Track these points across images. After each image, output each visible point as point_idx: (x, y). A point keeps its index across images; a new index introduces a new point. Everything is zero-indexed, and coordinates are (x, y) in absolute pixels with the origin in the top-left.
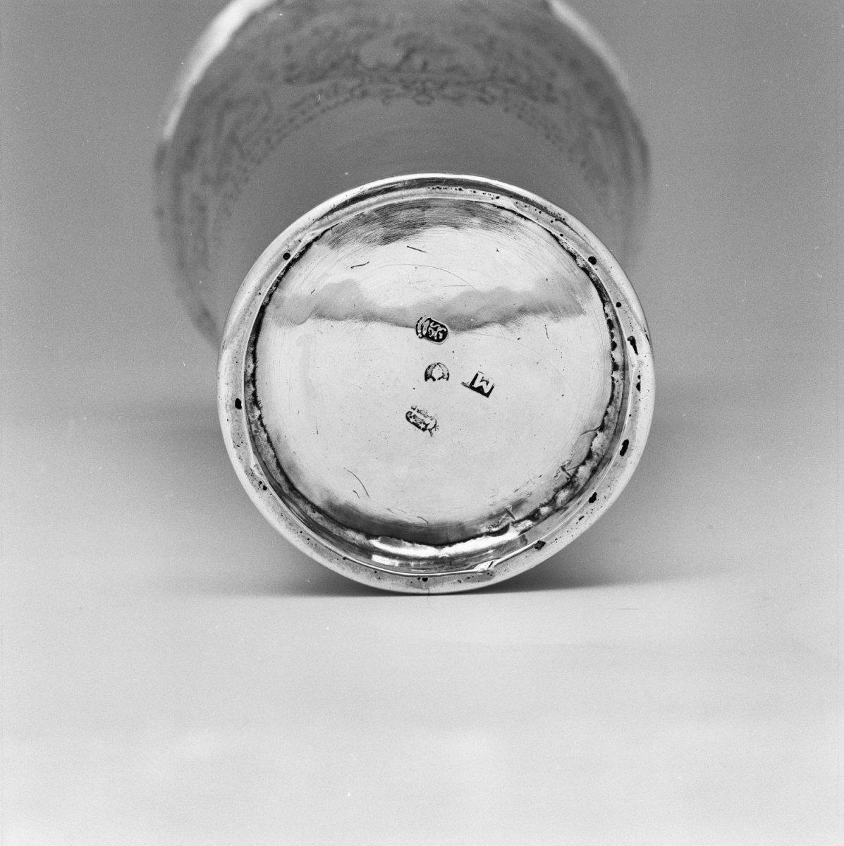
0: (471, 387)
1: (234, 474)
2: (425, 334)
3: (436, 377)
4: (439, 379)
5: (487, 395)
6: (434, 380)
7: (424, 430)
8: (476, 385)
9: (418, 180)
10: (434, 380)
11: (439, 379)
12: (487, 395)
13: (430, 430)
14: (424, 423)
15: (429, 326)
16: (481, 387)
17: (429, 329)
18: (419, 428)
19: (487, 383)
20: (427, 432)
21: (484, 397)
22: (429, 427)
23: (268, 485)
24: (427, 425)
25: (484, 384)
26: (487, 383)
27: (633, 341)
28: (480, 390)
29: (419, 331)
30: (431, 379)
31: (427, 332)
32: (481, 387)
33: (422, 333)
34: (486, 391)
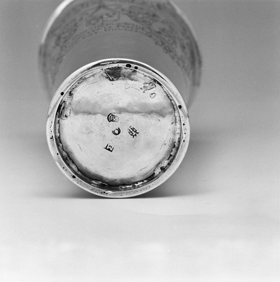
0: (106, 148)
1: (71, 74)
2: (120, 110)
3: (116, 130)
4: (115, 130)
5: (111, 151)
6: (116, 129)
7: (131, 135)
8: (108, 148)
9: (136, 63)
10: (116, 129)
11: (115, 130)
12: (111, 151)
13: (133, 136)
14: (132, 133)
15: (112, 117)
16: (109, 149)
17: (113, 118)
18: (130, 134)
19: (111, 147)
20: (132, 136)
21: (110, 152)
22: (133, 134)
23: (59, 153)
24: (133, 134)
25: (110, 147)
26: (111, 147)
27: (74, 177)
28: (109, 150)
29: (109, 119)
30: (117, 129)
31: (112, 119)
32: (109, 149)
33: (110, 120)
34: (111, 150)
